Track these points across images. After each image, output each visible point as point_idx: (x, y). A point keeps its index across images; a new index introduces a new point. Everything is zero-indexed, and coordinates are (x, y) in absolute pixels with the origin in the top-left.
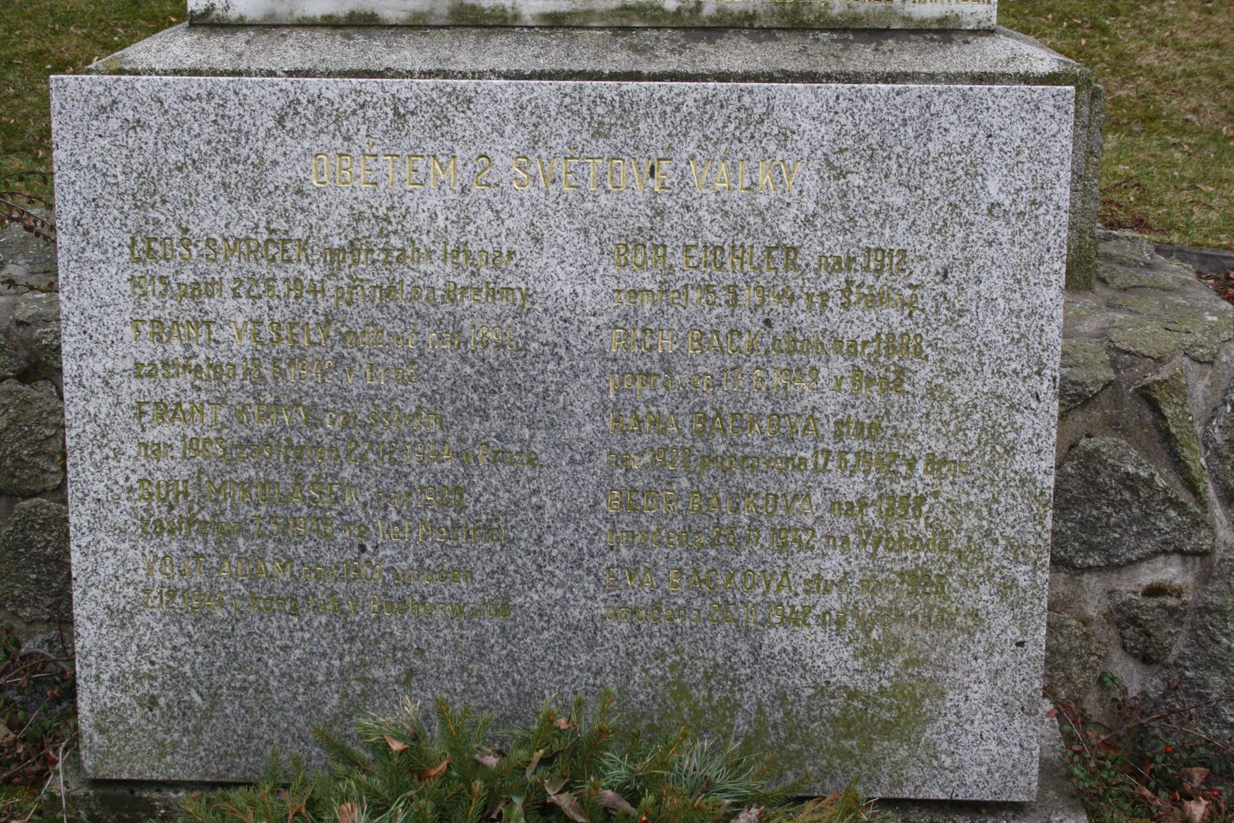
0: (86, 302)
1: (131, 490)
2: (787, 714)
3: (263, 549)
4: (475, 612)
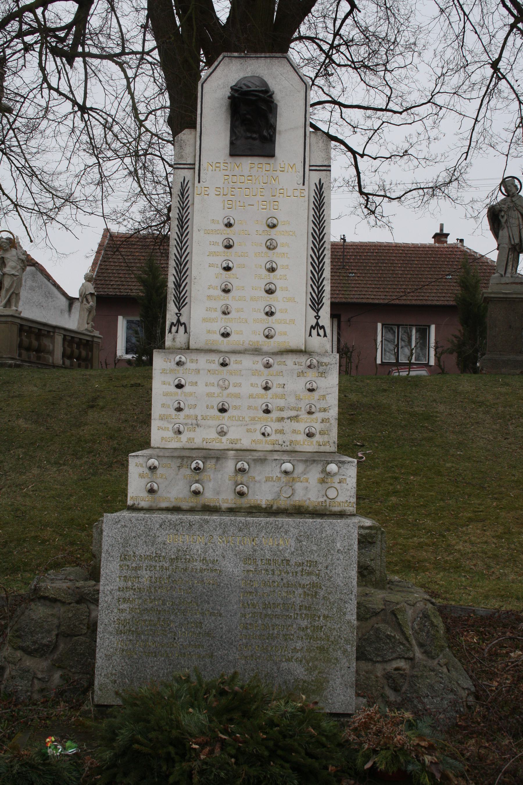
0: (107, 571)
1: (114, 622)
2: (287, 687)
3: (148, 639)
4: (203, 657)
